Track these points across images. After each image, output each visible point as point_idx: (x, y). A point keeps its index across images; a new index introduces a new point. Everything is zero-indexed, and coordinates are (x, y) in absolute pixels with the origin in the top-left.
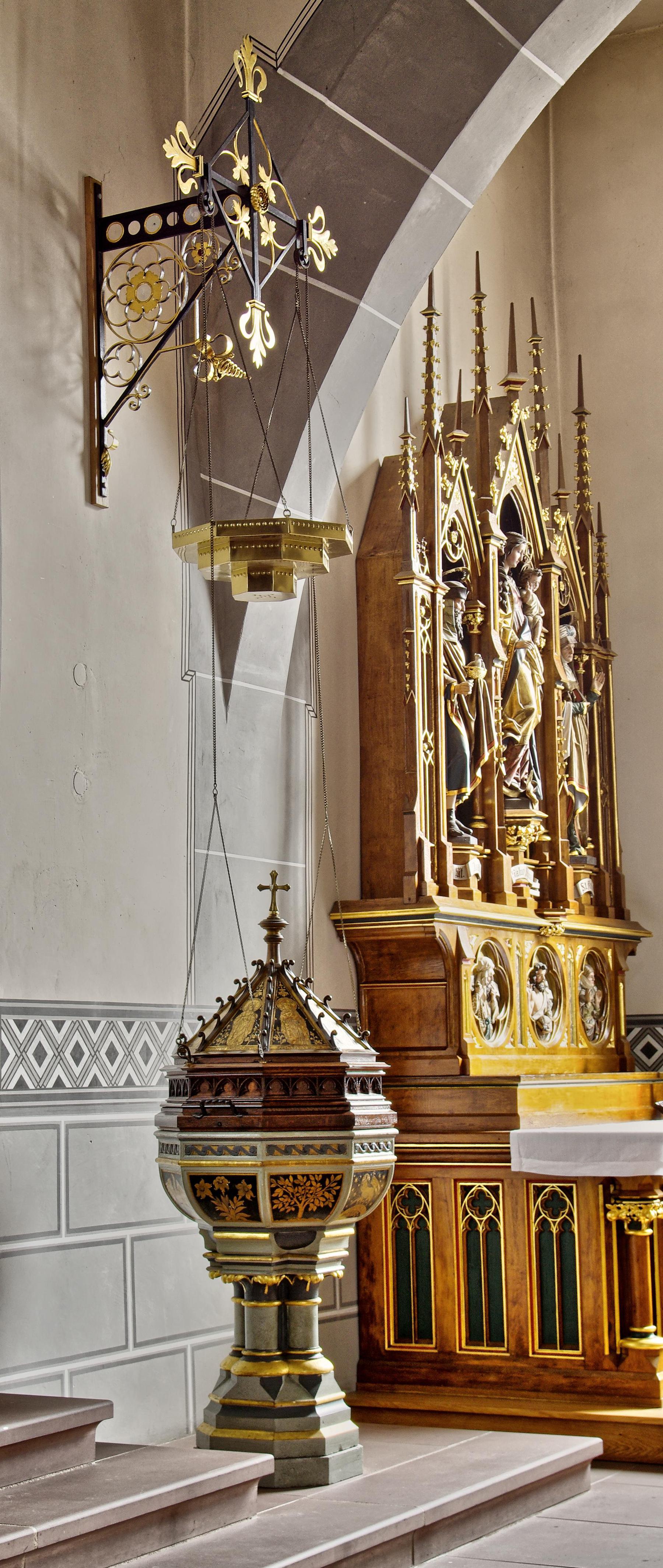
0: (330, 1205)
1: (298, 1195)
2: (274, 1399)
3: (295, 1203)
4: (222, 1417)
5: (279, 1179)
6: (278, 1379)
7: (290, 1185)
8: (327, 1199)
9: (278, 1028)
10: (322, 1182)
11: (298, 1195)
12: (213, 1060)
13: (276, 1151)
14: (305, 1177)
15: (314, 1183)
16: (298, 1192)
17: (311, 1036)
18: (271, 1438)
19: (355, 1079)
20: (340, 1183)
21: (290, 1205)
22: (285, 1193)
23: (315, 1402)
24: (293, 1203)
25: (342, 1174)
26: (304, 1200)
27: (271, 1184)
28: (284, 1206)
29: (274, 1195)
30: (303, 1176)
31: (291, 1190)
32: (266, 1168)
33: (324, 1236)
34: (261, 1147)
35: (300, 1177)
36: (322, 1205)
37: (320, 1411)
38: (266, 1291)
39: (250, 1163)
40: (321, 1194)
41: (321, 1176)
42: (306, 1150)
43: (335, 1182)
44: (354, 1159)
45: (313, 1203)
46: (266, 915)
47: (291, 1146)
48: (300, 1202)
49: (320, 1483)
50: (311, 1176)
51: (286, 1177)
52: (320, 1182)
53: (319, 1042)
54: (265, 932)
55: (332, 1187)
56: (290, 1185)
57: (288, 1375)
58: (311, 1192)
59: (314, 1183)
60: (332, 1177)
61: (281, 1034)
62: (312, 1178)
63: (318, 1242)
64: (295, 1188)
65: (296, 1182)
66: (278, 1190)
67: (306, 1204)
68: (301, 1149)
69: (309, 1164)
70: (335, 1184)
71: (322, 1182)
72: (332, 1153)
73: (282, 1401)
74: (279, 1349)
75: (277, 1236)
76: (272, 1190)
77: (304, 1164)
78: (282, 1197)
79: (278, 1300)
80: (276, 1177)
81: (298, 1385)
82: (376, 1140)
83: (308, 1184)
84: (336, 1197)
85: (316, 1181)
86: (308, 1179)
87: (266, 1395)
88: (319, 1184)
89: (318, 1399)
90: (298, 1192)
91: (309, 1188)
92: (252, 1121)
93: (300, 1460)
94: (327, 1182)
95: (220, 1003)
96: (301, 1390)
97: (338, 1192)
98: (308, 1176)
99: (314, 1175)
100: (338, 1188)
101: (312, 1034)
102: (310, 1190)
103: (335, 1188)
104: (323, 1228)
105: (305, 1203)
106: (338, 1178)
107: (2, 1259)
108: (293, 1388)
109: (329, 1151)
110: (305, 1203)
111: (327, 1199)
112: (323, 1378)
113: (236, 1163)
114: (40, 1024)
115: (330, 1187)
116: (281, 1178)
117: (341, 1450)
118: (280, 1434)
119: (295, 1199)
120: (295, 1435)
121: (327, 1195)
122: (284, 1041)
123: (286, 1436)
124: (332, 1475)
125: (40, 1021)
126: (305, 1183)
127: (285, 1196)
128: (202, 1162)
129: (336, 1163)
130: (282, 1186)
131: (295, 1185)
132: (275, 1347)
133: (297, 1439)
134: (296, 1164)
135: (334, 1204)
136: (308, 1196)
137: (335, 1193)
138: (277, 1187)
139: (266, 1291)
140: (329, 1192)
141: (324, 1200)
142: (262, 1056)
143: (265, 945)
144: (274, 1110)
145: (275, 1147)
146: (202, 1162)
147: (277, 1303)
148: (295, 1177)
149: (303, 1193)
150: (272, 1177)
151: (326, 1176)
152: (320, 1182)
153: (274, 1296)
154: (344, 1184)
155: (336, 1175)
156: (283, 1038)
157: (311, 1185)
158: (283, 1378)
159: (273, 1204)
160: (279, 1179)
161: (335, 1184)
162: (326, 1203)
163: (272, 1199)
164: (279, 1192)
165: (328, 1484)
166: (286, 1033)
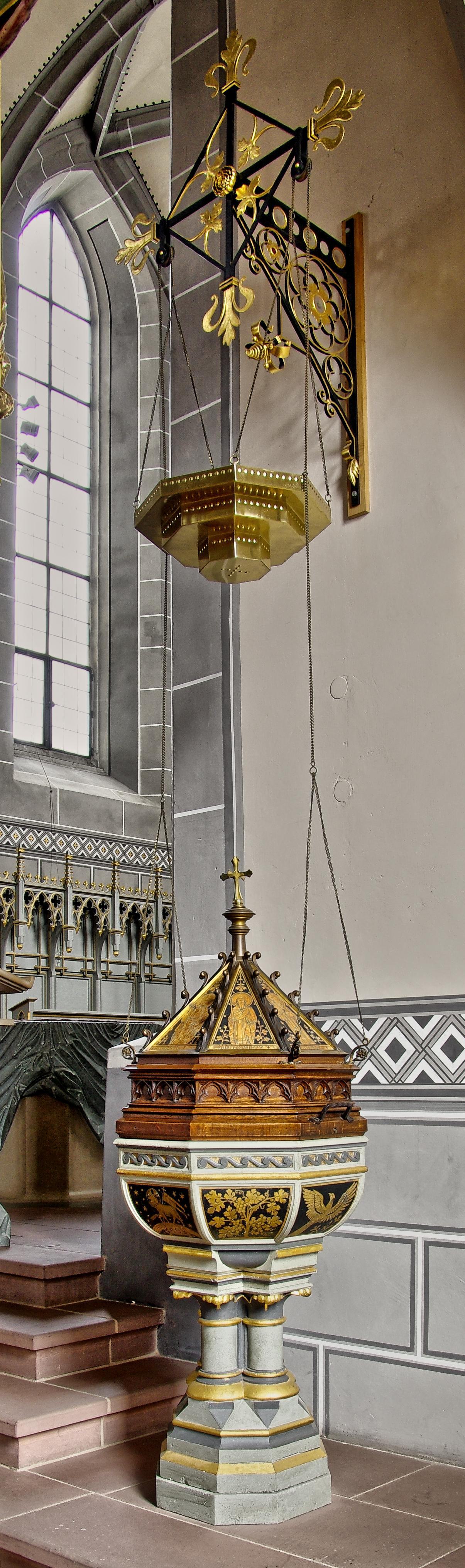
114: (396, 1021)
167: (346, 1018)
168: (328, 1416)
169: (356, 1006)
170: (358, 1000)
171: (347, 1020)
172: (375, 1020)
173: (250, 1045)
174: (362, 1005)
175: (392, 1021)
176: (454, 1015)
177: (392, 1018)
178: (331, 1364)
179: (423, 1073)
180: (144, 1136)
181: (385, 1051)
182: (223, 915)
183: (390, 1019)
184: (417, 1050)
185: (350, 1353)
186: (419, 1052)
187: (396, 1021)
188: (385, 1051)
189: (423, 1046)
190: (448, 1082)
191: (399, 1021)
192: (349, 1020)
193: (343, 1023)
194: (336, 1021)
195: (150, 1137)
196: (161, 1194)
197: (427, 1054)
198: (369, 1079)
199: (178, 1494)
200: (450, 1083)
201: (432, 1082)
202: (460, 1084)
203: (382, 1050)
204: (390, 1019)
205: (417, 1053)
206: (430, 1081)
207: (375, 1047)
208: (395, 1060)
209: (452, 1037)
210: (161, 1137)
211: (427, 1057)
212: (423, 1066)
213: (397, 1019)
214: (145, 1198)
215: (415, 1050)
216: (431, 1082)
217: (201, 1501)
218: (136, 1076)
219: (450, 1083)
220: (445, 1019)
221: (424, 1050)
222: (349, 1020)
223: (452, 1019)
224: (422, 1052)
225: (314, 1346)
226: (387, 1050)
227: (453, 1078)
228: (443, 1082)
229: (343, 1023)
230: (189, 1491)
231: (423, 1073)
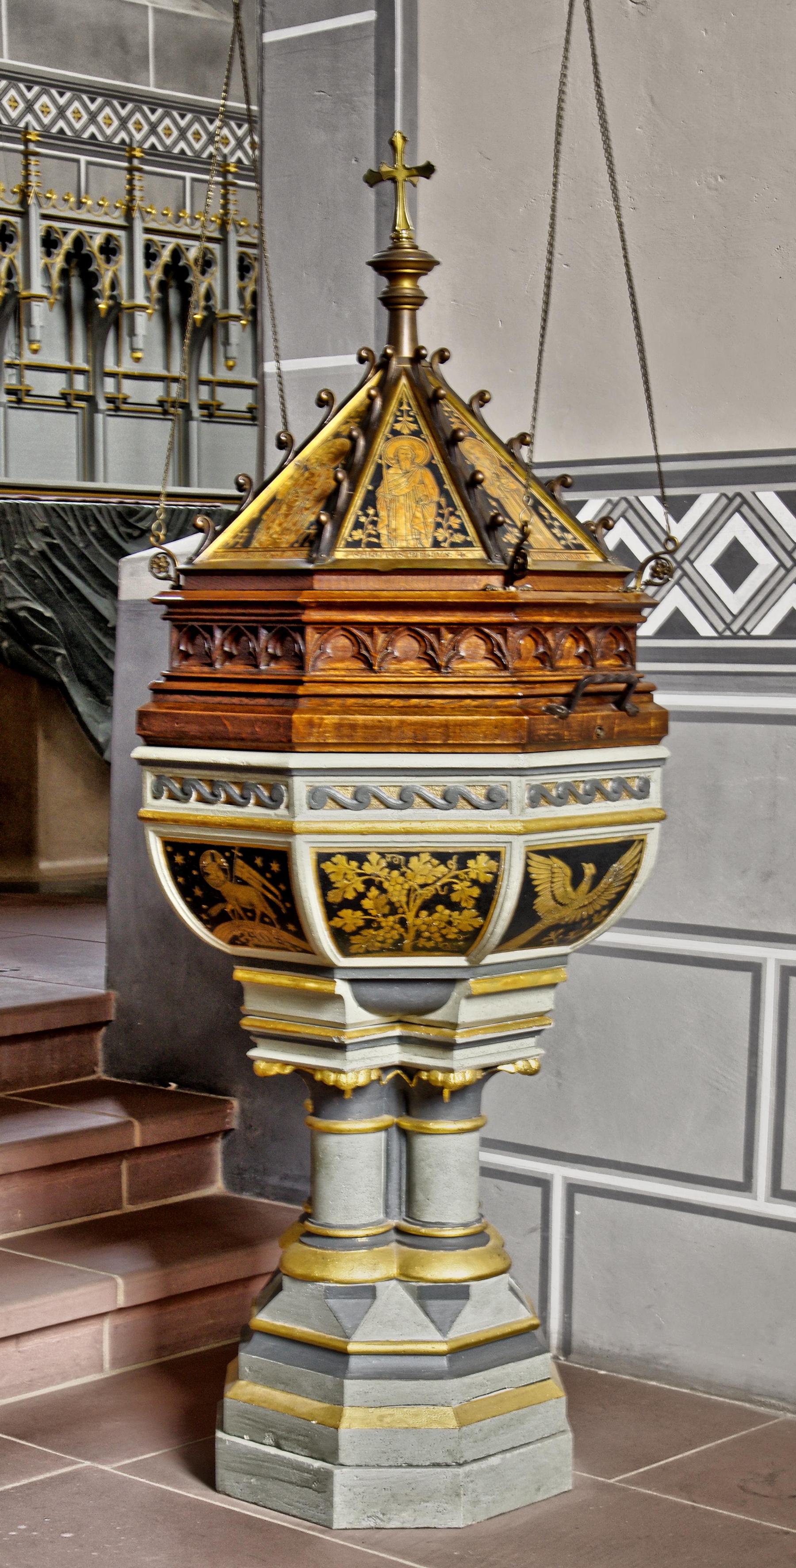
114: (738, 500)
117: (278, 1446)
167: (630, 494)
169: (652, 467)
171: (631, 498)
174: (666, 467)
177: (730, 495)
179: (677, 614)
180: (208, 743)
187: (738, 500)
193: (623, 505)
195: (208, 743)
205: (782, 572)
210: (233, 744)
215: (695, 564)
216: (692, 633)
217: (307, 1480)
231: (677, 614)
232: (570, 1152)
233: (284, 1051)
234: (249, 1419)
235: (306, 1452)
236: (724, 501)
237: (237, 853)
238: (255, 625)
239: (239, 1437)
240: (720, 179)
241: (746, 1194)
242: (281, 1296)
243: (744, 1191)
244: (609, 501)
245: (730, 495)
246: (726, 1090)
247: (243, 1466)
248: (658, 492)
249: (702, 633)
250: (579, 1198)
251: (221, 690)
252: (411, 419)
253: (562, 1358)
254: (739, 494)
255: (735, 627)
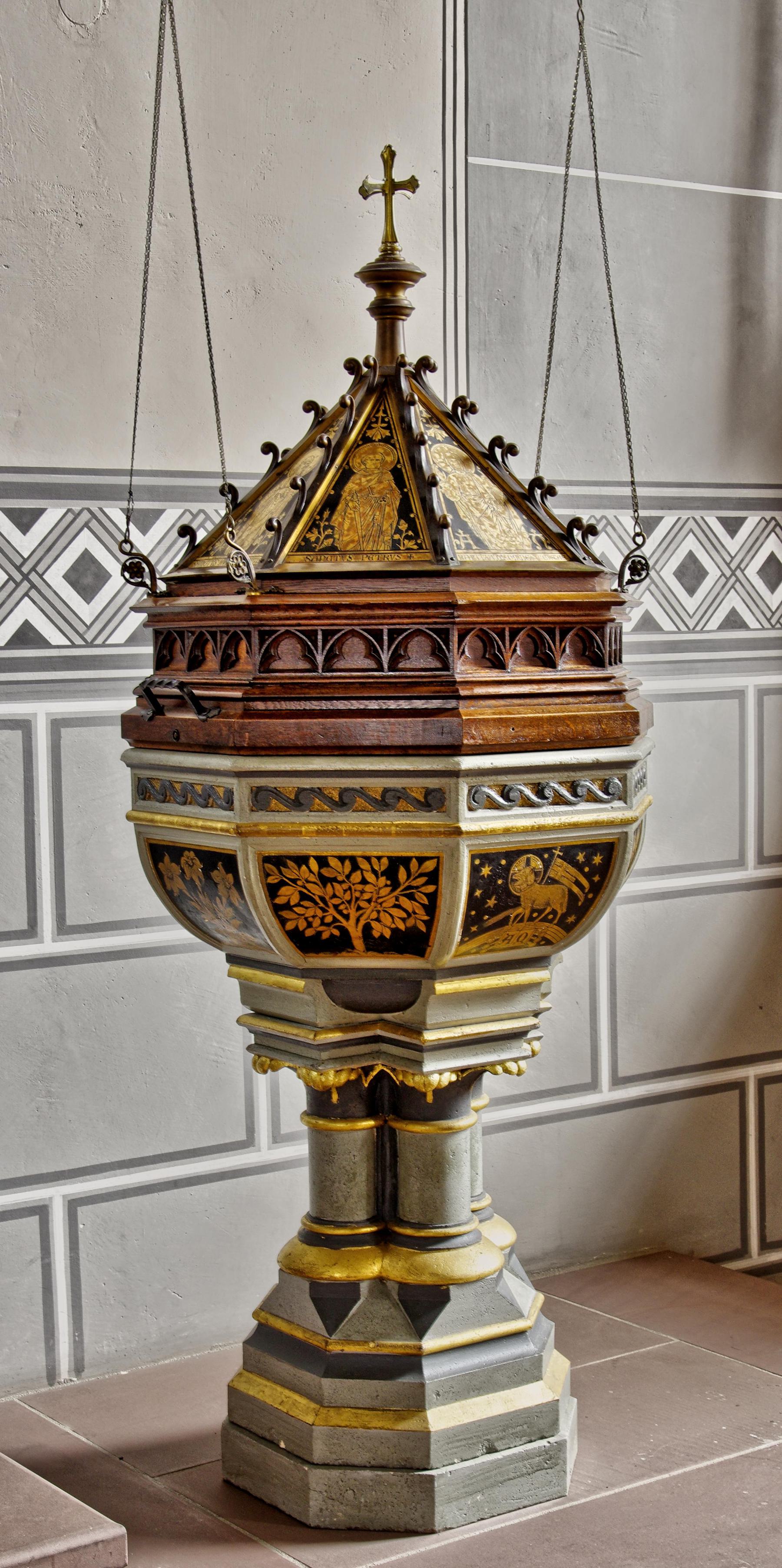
0: (423, 928)
1: (336, 901)
2: (330, 1334)
3: (335, 920)
4: (251, 1349)
5: (286, 866)
6: (351, 1289)
7: (312, 878)
8: (409, 915)
9: (326, 514)
10: (391, 873)
11: (336, 901)
12: (213, 587)
13: (274, 802)
14: (347, 863)
15: (370, 877)
16: (334, 896)
17: (398, 531)
18: (309, 1419)
19: (501, 635)
20: (433, 877)
21: (323, 923)
22: (304, 897)
23: (420, 1348)
24: (329, 919)
25: (438, 858)
26: (353, 914)
27: (267, 875)
28: (310, 925)
29: (278, 901)
30: (342, 859)
31: (316, 890)
32: (250, 839)
33: (433, 990)
34: (241, 790)
35: (333, 862)
36: (402, 927)
37: (431, 1370)
38: (335, 1097)
39: (219, 825)
40: (392, 901)
41: (385, 861)
42: (345, 800)
43: (421, 875)
44: (464, 826)
45: (378, 920)
46: (372, 254)
47: (312, 790)
48: (347, 917)
49: (412, 1526)
50: (360, 860)
51: (301, 860)
52: (383, 874)
53: (410, 544)
54: (370, 294)
55: (417, 887)
56: (312, 878)
57: (380, 1280)
58: (366, 896)
59: (370, 877)
60: (414, 864)
61: (326, 528)
62: (365, 865)
63: (425, 1004)
64: (325, 886)
65: (325, 872)
66: (284, 890)
67: (362, 922)
68: (336, 797)
69: (351, 833)
70: (423, 880)
71: (391, 873)
72: (411, 808)
73: (348, 1341)
74: (371, 1221)
75: (327, 984)
76: (272, 891)
77: (337, 833)
78: (298, 905)
79: (369, 1116)
80: (278, 861)
81: (395, 1305)
82: (565, 776)
83: (356, 877)
84: (431, 908)
85: (374, 872)
86: (355, 867)
87: (318, 1324)
88: (383, 880)
89: (429, 1343)
90: (334, 896)
91: (360, 887)
92: (220, 730)
93: (367, 1473)
94: (402, 874)
95: (271, 455)
96: (399, 1316)
97: (433, 898)
98: (353, 859)
99: (368, 859)
100: (431, 889)
101: (404, 526)
102: (362, 892)
103: (423, 889)
104: (432, 975)
105: (358, 920)
106: (429, 866)
107: (779, 853)
108: (384, 1309)
109: (402, 804)
110: (358, 920)
111: (409, 915)
112: (454, 1291)
113: (200, 823)
114: (773, 523)
115: (409, 887)
116: (290, 863)
117: (491, 1450)
118: (332, 1412)
119: (332, 911)
120: (368, 1418)
121: (405, 902)
122: (330, 541)
123: (345, 1417)
124: (443, 1513)
125: (773, 518)
126: (348, 877)
127: (304, 903)
128: (158, 817)
129: (415, 832)
130: (294, 881)
131: (324, 881)
132: (361, 1215)
133: (365, 1427)
134: (318, 832)
135: (429, 924)
136: (363, 904)
137: (425, 901)
138: (282, 884)
139: (335, 1097)
140: (411, 897)
141: (404, 915)
142: (254, 576)
143: (371, 325)
144: (271, 706)
145: (276, 793)
146: (158, 817)
147: (371, 1123)
148: (322, 861)
149: (347, 897)
150: (267, 859)
151: (397, 863)
152: (383, 874)
153: (358, 1107)
154: (444, 879)
155: (421, 860)
156: (327, 537)
157: (364, 882)
158: (364, 1288)
159: (283, 922)
160: (286, 866)
161: (423, 880)
162: (410, 922)
163: (277, 909)
164: (288, 894)
165: (433, 1532)
166: (341, 524)
167: (94, 506)
168: (81, 1335)
169: (124, 480)
170: (223, 472)
171: (95, 509)
172: (159, 513)
173: (525, 551)
174: (137, 481)
175: (768, 523)
176: (694, 518)
177: (195, 511)
178: (81, 1226)
179: (27, 625)
180: (536, 747)
181: (63, 577)
182: (423, 275)
183: (191, 513)
184: (11, 578)
185: (124, 1190)
186: (14, 581)
187: (202, 517)
188: (63, 577)
189: (25, 569)
190: (78, 641)
191: (609, 523)
192: (101, 509)
193: (86, 516)
194: (69, 511)
195: (558, 745)
196: (547, 864)
197: (33, 586)
198: (648, 623)
199: (488, 1478)
200: (83, 643)
201: (45, 644)
202: (104, 645)
203: (56, 576)
204: (191, 513)
205: (12, 585)
206: (41, 642)
207: (742, 566)
208: (691, 591)
209: (691, 555)
210: (567, 746)
211: (33, 593)
212: (733, 601)
213: (776, 520)
214: (505, 878)
215: (45, 577)
216: (43, 643)
217: (539, 1464)
218: (400, 617)
219: (83, 643)
220: (70, 517)
221: (26, 577)
222: (702, 518)
223: (691, 524)
224: (22, 581)
225: (41, 1203)
226: (762, 572)
227: (89, 637)
228: (69, 643)
229: (86, 516)
230: (511, 1459)
231: (27, 625)
232: (117, 1160)
233: (456, 1057)
234: (461, 1440)
235: (524, 1439)
236: (763, 523)
237: (557, 852)
238: (552, 626)
239: (450, 1464)
240: (169, 217)
241: (251, 1148)
242: (449, 1308)
243: (248, 1147)
244: (763, 518)
245: (195, 511)
246: (225, 1060)
247: (466, 1489)
248: (125, 505)
249: (666, 628)
250: (34, 1221)
251: (544, 691)
252: (385, 425)
253: (75, 1379)
254: (773, 518)
255: (773, 621)
